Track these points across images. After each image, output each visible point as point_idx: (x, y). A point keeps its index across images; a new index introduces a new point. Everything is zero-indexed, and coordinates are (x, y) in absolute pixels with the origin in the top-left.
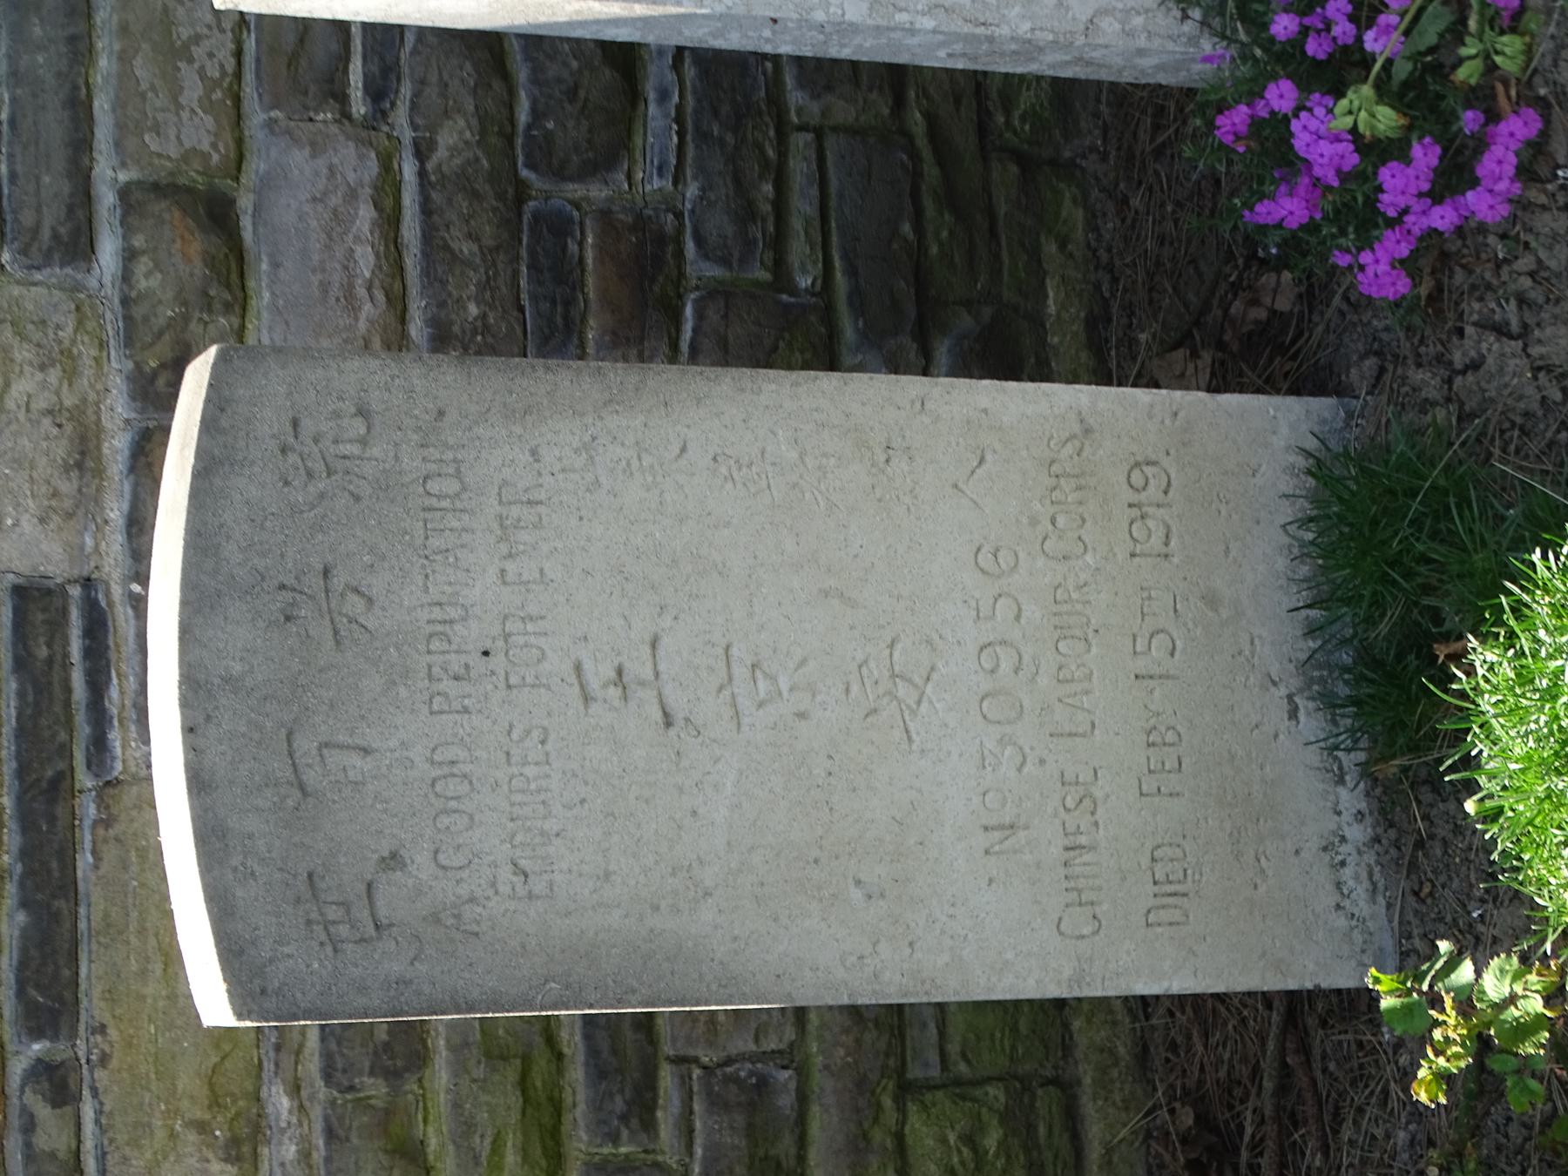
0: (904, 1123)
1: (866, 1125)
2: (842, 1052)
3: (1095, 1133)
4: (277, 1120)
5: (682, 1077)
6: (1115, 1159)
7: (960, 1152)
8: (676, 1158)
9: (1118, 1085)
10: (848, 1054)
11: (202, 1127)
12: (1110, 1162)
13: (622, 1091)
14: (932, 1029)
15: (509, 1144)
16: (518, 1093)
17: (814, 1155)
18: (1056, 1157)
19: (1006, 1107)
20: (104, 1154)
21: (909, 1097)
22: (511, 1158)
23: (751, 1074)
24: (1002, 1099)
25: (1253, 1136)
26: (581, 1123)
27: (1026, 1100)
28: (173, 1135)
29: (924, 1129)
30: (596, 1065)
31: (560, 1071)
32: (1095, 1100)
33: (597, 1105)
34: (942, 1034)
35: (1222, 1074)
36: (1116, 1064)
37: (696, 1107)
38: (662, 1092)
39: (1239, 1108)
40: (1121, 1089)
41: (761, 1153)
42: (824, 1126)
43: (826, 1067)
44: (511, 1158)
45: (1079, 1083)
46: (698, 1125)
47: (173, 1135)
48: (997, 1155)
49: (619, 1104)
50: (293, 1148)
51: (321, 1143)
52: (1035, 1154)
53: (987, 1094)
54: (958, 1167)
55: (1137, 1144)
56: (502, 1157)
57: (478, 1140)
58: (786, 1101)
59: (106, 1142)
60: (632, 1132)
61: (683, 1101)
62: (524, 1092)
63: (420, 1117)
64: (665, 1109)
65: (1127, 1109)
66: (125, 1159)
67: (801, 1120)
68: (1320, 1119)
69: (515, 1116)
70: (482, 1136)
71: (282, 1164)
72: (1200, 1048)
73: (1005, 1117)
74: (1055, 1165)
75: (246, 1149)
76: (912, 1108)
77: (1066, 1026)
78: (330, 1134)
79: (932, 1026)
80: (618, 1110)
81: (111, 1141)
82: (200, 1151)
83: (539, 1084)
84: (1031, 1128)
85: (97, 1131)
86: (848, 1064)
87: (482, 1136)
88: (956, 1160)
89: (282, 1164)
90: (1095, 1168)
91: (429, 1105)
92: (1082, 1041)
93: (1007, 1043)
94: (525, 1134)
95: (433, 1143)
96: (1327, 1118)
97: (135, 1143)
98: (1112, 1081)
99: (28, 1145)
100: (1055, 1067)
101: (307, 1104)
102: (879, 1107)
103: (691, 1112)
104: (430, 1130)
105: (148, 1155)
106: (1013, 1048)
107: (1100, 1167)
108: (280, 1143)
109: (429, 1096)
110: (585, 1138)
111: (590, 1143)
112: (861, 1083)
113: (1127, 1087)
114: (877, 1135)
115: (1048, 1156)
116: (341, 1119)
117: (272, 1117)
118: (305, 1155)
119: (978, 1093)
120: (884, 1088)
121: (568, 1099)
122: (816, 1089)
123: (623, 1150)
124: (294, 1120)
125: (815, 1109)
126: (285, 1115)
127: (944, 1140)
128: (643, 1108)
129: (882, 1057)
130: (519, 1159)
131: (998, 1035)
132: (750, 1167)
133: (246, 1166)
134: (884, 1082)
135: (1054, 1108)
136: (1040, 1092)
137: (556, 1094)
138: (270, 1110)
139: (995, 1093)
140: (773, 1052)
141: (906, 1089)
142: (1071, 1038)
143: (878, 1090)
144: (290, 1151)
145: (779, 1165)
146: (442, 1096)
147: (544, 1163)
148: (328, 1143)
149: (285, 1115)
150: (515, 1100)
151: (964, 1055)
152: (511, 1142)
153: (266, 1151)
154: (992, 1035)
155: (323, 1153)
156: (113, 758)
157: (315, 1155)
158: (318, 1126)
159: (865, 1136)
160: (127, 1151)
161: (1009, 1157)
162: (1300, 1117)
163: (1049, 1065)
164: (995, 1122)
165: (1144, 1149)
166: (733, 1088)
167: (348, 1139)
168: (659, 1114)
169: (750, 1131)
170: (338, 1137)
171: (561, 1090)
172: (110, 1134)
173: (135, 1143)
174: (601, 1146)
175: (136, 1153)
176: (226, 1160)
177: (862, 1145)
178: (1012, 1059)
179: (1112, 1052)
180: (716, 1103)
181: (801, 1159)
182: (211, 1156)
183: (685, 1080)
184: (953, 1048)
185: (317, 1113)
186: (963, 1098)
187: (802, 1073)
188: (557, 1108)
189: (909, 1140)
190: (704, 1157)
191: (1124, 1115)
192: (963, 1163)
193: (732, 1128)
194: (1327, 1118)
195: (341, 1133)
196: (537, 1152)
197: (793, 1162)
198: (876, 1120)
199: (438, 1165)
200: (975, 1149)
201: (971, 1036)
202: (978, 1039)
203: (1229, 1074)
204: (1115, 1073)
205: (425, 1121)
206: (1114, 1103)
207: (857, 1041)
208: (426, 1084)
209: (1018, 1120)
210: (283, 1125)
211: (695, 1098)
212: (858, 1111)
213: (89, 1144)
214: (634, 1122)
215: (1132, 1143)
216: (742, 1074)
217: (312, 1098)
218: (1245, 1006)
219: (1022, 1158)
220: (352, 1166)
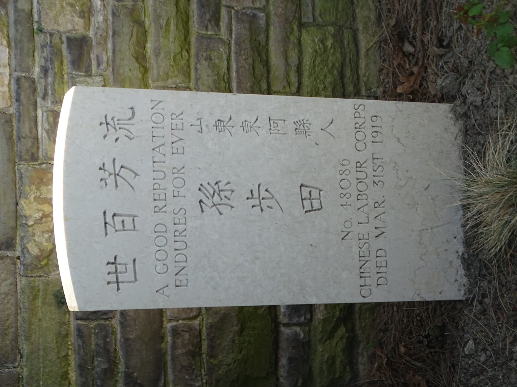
0: (301, 36)
1: (288, 34)
2: (281, 9)
3: (363, 45)
4: (97, 8)
5: (228, 12)
6: (370, 54)
7: (319, 45)
8: (226, 37)
9: (371, 28)
10: (282, 10)
11: (72, 5)
12: (368, 55)
13: (209, 12)
14: (310, 8)
15: (172, 23)
16: (175, 7)
17: (271, 42)
18: (350, 51)
19: (334, 33)
20: (40, 12)
21: (302, 28)
22: (172, 28)
23: (251, 13)
24: (333, 30)
25: (414, 27)
26: (195, 21)
27: (341, 33)
28: (62, 7)
29: (307, 38)
30: (200, 3)
31: (189, 5)
32: (363, 33)
33: (201, 16)
34: (313, 9)
35: (404, 12)
36: (370, 21)
37: (233, 22)
38: (222, 17)
39: (409, 21)
40: (372, 29)
41: (254, 38)
42: (274, 33)
43: (276, 14)
44: (172, 28)
45: (358, 30)
46: (233, 28)
47: (62, 7)
48: (331, 48)
49: (208, 16)
50: (102, 18)
51: (111, 18)
52: (343, 50)
53: (328, 29)
54: (318, 50)
55: (377, 48)
56: (170, 27)
57: (162, 21)
58: (262, 22)
59: (41, 8)
60: (212, 26)
61: (228, 19)
62: (177, 7)
63: (143, 13)
64: (223, 22)
65: (374, 36)
66: (47, 14)
67: (267, 31)
68: (435, 9)
69: (174, 14)
70: (163, 20)
71: (98, 22)
72: (397, 5)
73: (334, 36)
74: (350, 54)
75: (86, 15)
76: (304, 31)
77: (354, 11)
78: (114, 14)
79: (310, 5)
80: (207, 18)
81: (42, 8)
82: (71, 13)
83: (182, 7)
84: (342, 42)
85: (38, 5)
86: (283, 13)
87: (163, 20)
88: (317, 47)
89: (98, 22)
90: (363, 57)
91: (146, 11)
92: (359, 16)
93: (334, 13)
94: (177, 20)
95: (147, 23)
96: (438, 8)
97: (50, 9)
98: (369, 27)
99: (15, 7)
100: (351, 24)
101: (106, 6)
102: (292, 29)
103: (231, 24)
104: (146, 19)
105: (55, 13)
106: (337, 14)
107: (365, 56)
108: (98, 15)
109: (146, 8)
110: (197, 26)
111: (198, 29)
112: (287, 20)
113: (374, 29)
114: (292, 38)
115: (348, 51)
116: (117, 10)
117: (95, 7)
118: (106, 20)
119: (325, 28)
120: (294, 23)
121: (191, 14)
122: (272, 21)
123: (209, 33)
124: (102, 8)
125: (272, 28)
126: (99, 7)
127: (314, 41)
128: (216, 19)
129: (294, 12)
130: (175, 28)
131: (332, 10)
132: (250, 41)
133: (86, 20)
134: (294, 21)
135: (350, 36)
136: (345, 31)
137: (187, 11)
138: (94, 4)
139: (331, 29)
140: (258, 8)
141: (301, 25)
142: (356, 15)
143: (292, 23)
144: (101, 18)
145: (259, 43)
146: (150, 8)
147: (183, 31)
148: (113, 17)
149: (99, 7)
150: (174, 9)
151: (320, 16)
152: (173, 22)
153: (93, 19)
154: (330, 10)
155: (111, 20)
156: (123, 356)
157: (109, 22)
158: (110, 12)
159: (288, 37)
160: (48, 11)
161: (335, 49)
162: (429, 14)
163: (348, 23)
164: (330, 37)
165: (379, 50)
166: (245, 16)
167: (119, 17)
168: (221, 24)
169: (250, 29)
170: (117, 16)
171: (189, 11)
172: (42, 6)
173: (50, 9)
174: (201, 30)
175: (50, 12)
176: (80, 17)
177: (287, 40)
178: (336, 18)
179: (369, 17)
180: (239, 20)
181: (267, 44)
182: (75, 16)
183: (229, 13)
184: (317, 14)
185: (109, 9)
186: (320, 29)
187: (268, 16)
188: (188, 17)
189: (302, 42)
190: (236, 38)
191: (372, 38)
192: (320, 49)
193: (244, 28)
194: (438, 8)
195: (117, 14)
196: (181, 27)
197: (264, 44)
198: (291, 33)
199: (149, 30)
200: (324, 45)
201: (323, 10)
202: (325, 10)
203: (407, 12)
204: (370, 24)
205: (145, 15)
206: (369, 34)
207: (286, 6)
208: (145, 3)
209: (338, 37)
210: (99, 10)
211: (233, 19)
212: (286, 29)
213: (35, 10)
214: (213, 22)
215: (375, 48)
216: (248, 13)
217: (108, 4)
218: (428, 358)
219: (339, 50)
220: (121, 25)
